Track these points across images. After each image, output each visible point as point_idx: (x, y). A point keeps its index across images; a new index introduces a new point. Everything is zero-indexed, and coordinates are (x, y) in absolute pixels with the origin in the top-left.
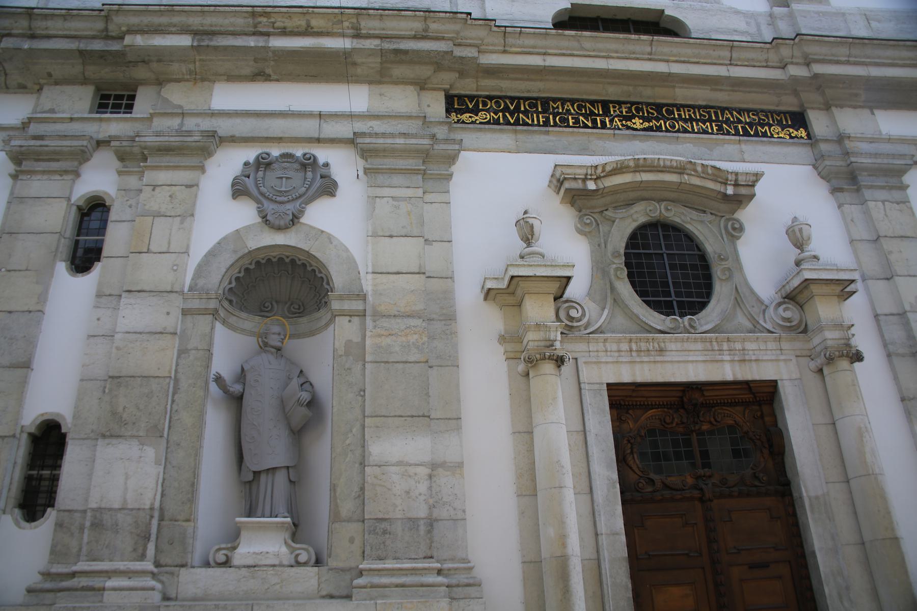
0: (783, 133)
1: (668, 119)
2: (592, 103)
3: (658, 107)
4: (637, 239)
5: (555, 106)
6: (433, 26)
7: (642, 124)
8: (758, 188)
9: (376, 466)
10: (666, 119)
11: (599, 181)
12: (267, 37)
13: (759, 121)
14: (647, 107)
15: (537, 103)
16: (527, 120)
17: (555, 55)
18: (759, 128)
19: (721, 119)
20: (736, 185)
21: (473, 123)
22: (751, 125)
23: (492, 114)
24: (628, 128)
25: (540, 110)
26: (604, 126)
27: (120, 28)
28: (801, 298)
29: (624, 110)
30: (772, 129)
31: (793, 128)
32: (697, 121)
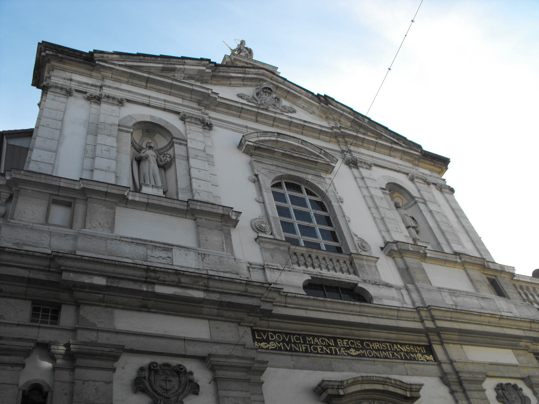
0: (423, 357)
1: (368, 349)
2: (328, 338)
3: (362, 342)
5: (309, 340)
6: (250, 289)
7: (355, 352)
8: (421, 393)
10: (367, 349)
11: (344, 390)
12: (153, 286)
13: (411, 351)
14: (356, 342)
15: (300, 337)
16: (296, 348)
18: (411, 355)
19: (393, 349)
21: (267, 349)
23: (277, 344)
25: (302, 342)
26: (336, 354)
27: (60, 267)
31: (427, 355)
32: (382, 350)
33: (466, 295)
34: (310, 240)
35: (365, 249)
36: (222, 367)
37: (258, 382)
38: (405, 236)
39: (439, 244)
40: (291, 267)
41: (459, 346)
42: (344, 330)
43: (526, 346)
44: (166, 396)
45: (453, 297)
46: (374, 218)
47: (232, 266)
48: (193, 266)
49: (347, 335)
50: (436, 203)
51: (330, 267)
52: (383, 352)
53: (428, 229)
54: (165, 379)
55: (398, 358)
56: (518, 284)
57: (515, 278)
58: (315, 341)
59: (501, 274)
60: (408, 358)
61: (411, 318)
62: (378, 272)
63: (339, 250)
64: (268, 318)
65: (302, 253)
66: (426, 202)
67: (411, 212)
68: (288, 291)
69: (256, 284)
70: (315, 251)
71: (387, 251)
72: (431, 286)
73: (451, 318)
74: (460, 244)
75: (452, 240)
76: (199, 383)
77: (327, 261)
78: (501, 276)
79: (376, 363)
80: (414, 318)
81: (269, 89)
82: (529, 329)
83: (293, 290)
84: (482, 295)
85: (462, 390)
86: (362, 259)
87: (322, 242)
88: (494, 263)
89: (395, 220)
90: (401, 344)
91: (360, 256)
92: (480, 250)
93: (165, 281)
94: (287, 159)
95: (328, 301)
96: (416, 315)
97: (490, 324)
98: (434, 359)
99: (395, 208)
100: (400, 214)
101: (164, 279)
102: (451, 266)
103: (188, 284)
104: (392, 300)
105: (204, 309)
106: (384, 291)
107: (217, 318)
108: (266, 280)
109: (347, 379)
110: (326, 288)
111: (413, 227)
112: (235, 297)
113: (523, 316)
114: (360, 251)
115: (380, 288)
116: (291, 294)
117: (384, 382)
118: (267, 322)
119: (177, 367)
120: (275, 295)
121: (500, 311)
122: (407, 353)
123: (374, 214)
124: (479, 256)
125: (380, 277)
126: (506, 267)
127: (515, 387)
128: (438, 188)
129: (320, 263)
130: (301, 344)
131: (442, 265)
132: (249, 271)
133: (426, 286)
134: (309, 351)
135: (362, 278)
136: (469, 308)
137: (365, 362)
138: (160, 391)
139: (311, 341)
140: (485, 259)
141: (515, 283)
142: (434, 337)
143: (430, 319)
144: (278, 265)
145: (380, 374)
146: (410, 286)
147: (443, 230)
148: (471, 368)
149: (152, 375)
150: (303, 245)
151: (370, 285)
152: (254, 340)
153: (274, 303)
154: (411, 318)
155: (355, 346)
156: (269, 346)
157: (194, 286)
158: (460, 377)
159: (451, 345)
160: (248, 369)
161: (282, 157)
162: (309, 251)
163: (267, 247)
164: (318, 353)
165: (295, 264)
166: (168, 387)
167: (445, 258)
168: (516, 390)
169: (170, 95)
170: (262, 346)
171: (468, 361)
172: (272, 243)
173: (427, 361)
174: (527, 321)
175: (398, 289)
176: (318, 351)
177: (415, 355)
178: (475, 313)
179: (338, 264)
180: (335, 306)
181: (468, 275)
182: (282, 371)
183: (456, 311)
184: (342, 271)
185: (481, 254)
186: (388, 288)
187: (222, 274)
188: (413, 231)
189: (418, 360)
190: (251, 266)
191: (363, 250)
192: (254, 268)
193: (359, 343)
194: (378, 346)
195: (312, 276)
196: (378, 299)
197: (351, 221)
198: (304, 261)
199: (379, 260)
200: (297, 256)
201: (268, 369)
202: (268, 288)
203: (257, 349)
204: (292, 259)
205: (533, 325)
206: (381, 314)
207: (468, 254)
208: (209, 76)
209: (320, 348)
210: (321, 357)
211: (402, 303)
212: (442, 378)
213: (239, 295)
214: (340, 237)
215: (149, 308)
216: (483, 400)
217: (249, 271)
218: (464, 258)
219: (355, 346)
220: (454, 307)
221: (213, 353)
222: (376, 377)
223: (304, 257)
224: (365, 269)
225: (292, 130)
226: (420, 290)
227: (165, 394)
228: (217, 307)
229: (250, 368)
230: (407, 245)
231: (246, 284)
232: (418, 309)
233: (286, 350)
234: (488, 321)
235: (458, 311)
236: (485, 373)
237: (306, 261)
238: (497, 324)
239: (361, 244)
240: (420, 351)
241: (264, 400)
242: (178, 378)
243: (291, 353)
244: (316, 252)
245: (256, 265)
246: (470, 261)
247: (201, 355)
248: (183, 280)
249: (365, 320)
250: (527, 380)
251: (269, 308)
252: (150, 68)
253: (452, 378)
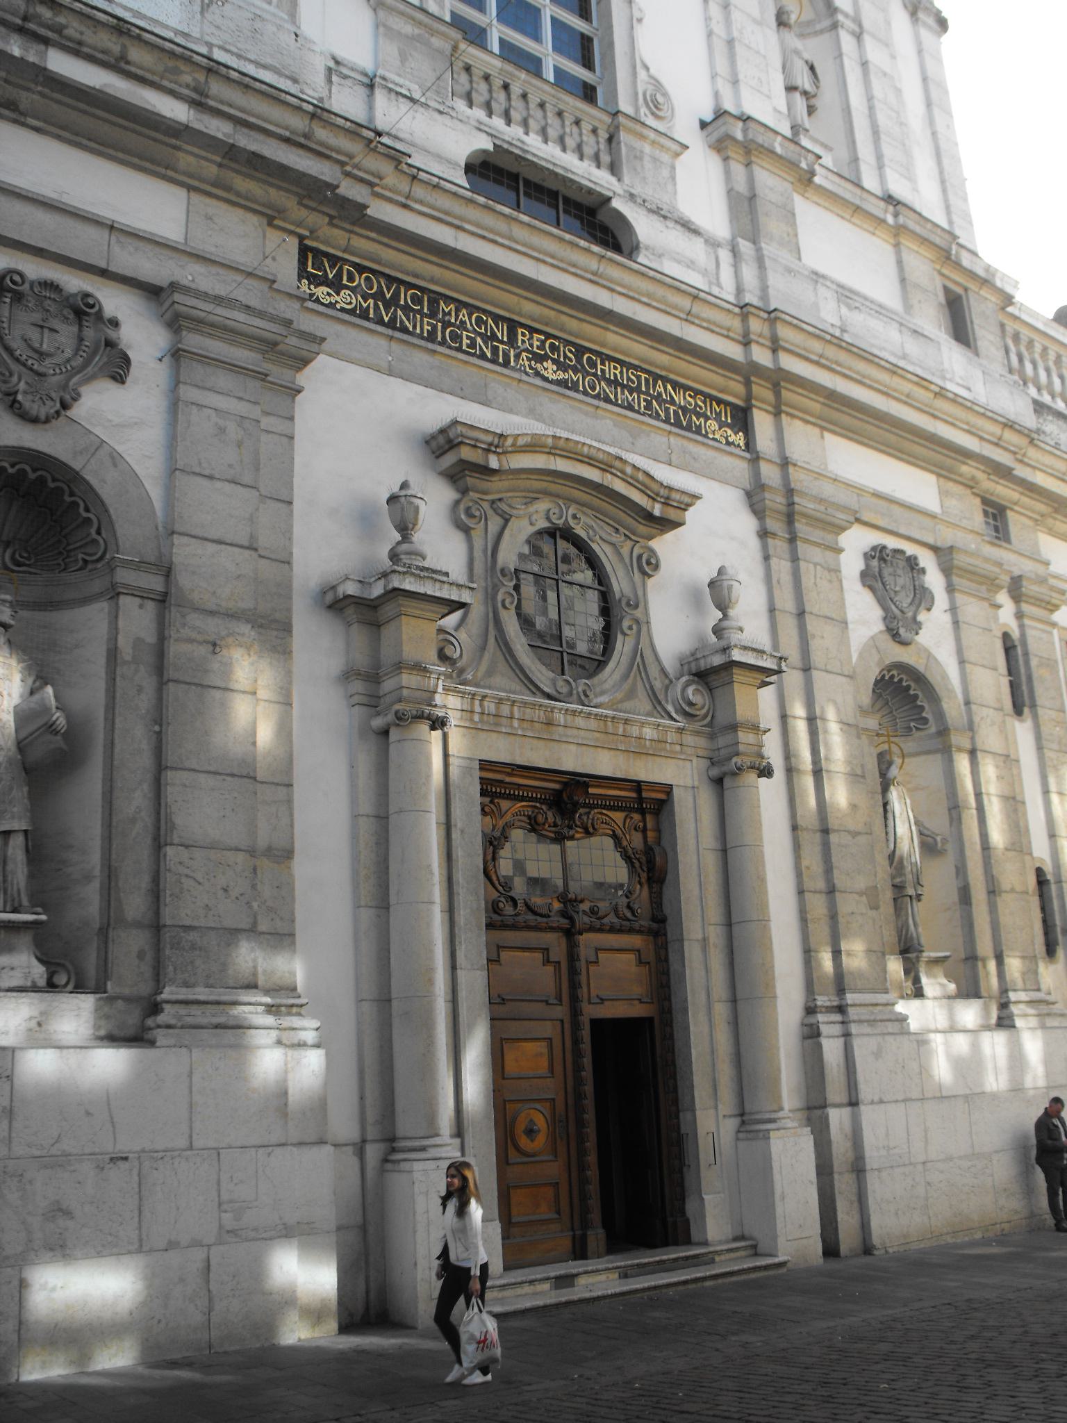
1: (588, 374)
2: (497, 318)
3: (580, 351)
5: (447, 310)
6: (321, 133)
7: (555, 372)
8: (690, 515)
9: (181, 845)
11: (503, 457)
12: (42, 47)
14: (564, 347)
15: (423, 297)
16: (407, 323)
17: (473, 234)
18: (694, 418)
21: (331, 305)
23: (360, 298)
24: (537, 374)
25: (426, 311)
26: (506, 364)
28: (714, 680)
29: (536, 343)
30: (708, 424)
32: (623, 386)
33: (877, 312)
34: (516, 40)
35: (657, 112)
36: (201, 325)
37: (290, 385)
38: (775, 110)
39: (855, 160)
40: (447, 103)
41: (817, 431)
42: (542, 308)
43: (973, 478)
44: (35, 367)
45: (842, 306)
46: (710, 34)
47: (285, 52)
48: (173, 22)
49: (547, 325)
50: (887, 45)
51: (553, 133)
52: (626, 392)
53: (843, 110)
54: (41, 323)
55: (657, 417)
56: (1011, 326)
57: (1010, 309)
58: (461, 316)
59: (980, 288)
60: (683, 422)
61: (722, 328)
62: (675, 185)
63: (588, 93)
64: (353, 224)
65: (485, 73)
66: (861, 33)
67: (813, 48)
68: (422, 167)
69: (340, 122)
70: (523, 75)
71: (716, 135)
72: (797, 262)
73: (821, 356)
74: (910, 177)
75: (891, 161)
76: (130, 353)
77: (549, 114)
78: (978, 293)
79: (600, 412)
80: (729, 330)
82: (995, 440)
83: (436, 168)
84: (915, 324)
85: (787, 536)
86: (642, 137)
87: (550, 59)
88: (975, 254)
89: (764, 57)
90: (676, 385)
91: (638, 128)
92: (952, 209)
93: (80, 43)
95: (522, 222)
96: (736, 324)
97: (907, 401)
98: (747, 445)
99: (773, 22)
100: (782, 43)
101: (77, 36)
102: (865, 226)
103: (148, 71)
104: (688, 267)
105: (180, 155)
106: (672, 238)
107: (214, 191)
108: (371, 118)
109: (517, 432)
110: (524, 186)
111: (805, 93)
112: (274, 142)
113: (994, 406)
114: (642, 114)
115: (667, 227)
116: (429, 176)
117: (606, 465)
118: (347, 235)
119: (79, 299)
120: (386, 168)
121: (944, 378)
122: (684, 409)
123: (714, 21)
124: (945, 225)
125: (675, 199)
126: (998, 275)
127: (912, 562)
128: (908, 5)
129: (529, 115)
130: (423, 315)
131: (843, 218)
132: (330, 81)
133: (785, 257)
134: (439, 339)
135: (626, 188)
136: (873, 345)
137: (571, 402)
138: (20, 350)
139: (449, 313)
140: (955, 237)
141: (1005, 321)
142: (762, 391)
143: (768, 343)
144: (414, 87)
145: (603, 443)
146: (745, 246)
147: (878, 126)
148: (828, 490)
149: (5, 303)
150: (496, 49)
151: (643, 212)
152: (303, 273)
153: (376, 189)
154: (722, 328)
155: (559, 356)
156: (338, 299)
157: (165, 83)
158: (793, 503)
159: (798, 423)
160: (269, 347)
162: (507, 72)
163: (395, 27)
164: (459, 349)
165: (460, 97)
166: (45, 346)
167: (858, 202)
168: (912, 569)
170: (321, 295)
171: (824, 473)
172: (413, 19)
173: (728, 443)
174: (996, 421)
175: (712, 243)
176: (461, 343)
177: (702, 420)
178: (883, 363)
179: (575, 129)
180: (536, 240)
181: (900, 263)
182: (356, 373)
183: (838, 342)
184: (580, 152)
185: (951, 222)
186: (687, 234)
187: (251, 69)
188: (800, 103)
189: (706, 436)
190: (336, 69)
191: (653, 114)
192: (345, 77)
193: (570, 351)
194: (617, 372)
195: (498, 142)
196: (653, 254)
197: (645, 21)
198: (486, 96)
199: (687, 153)
200: (470, 75)
201: (321, 357)
202: (371, 141)
203: (302, 300)
204: (457, 81)
205: (1008, 435)
206: (648, 295)
207: (918, 209)
209: (468, 337)
210: (466, 362)
211: (710, 283)
212: (749, 495)
213: (287, 140)
214: (602, 59)
215: (22, 114)
216: (830, 570)
217: (330, 81)
218: (906, 216)
219: (559, 356)
220: (837, 334)
221: (184, 282)
222: (590, 446)
223: (490, 85)
224: (642, 166)
226: (768, 263)
227: (34, 362)
228: (219, 159)
229: (276, 344)
230: (771, 135)
231: (313, 116)
232: (744, 309)
233: (380, 321)
234: (906, 391)
235: (844, 344)
236: (856, 512)
237: (491, 97)
238: (926, 406)
239: (651, 96)
240: (718, 415)
241: (293, 434)
242: (75, 329)
243: (390, 332)
244: (524, 81)
245: (352, 69)
246: (918, 229)
247: (151, 281)
248: (137, 54)
249: (603, 298)
250: (944, 555)
251: (360, 200)
253: (775, 500)
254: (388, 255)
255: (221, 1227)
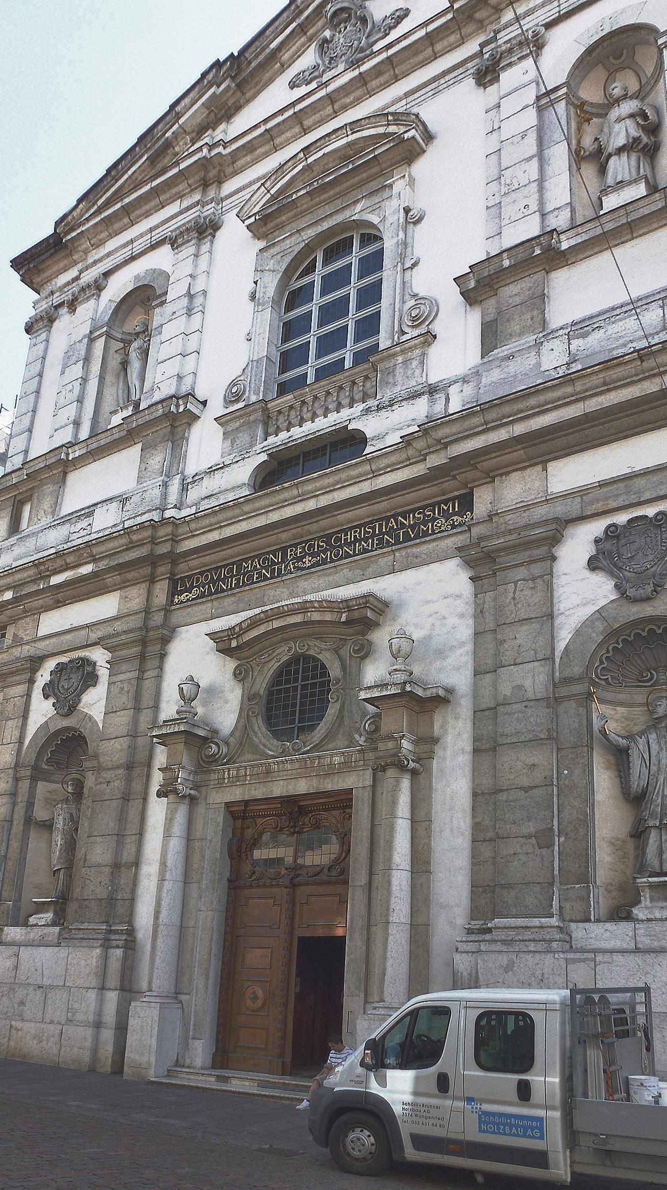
4: (284, 674)
6: (134, 537)
20: (350, 610)
22: (412, 527)
49: (302, 537)
81: (342, 9)
94: (323, 197)
161: (312, 200)
169: (163, 207)
187: (139, 520)
206: (338, 483)
208: (234, 93)
213: (127, 549)
225: (373, 90)
252: (134, 178)
254: (207, 559)
255: (67, 1018)
